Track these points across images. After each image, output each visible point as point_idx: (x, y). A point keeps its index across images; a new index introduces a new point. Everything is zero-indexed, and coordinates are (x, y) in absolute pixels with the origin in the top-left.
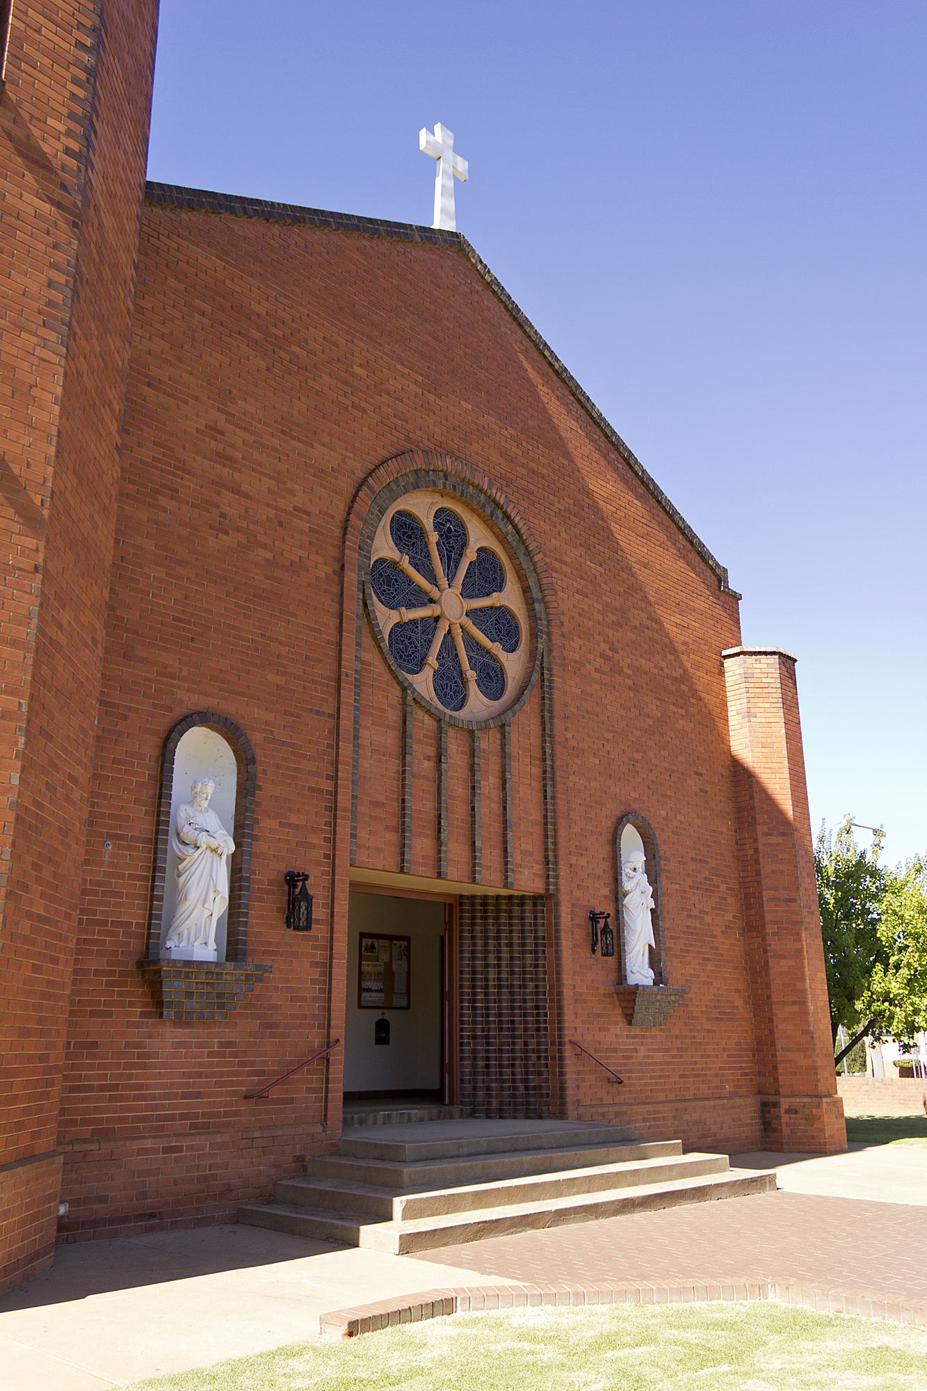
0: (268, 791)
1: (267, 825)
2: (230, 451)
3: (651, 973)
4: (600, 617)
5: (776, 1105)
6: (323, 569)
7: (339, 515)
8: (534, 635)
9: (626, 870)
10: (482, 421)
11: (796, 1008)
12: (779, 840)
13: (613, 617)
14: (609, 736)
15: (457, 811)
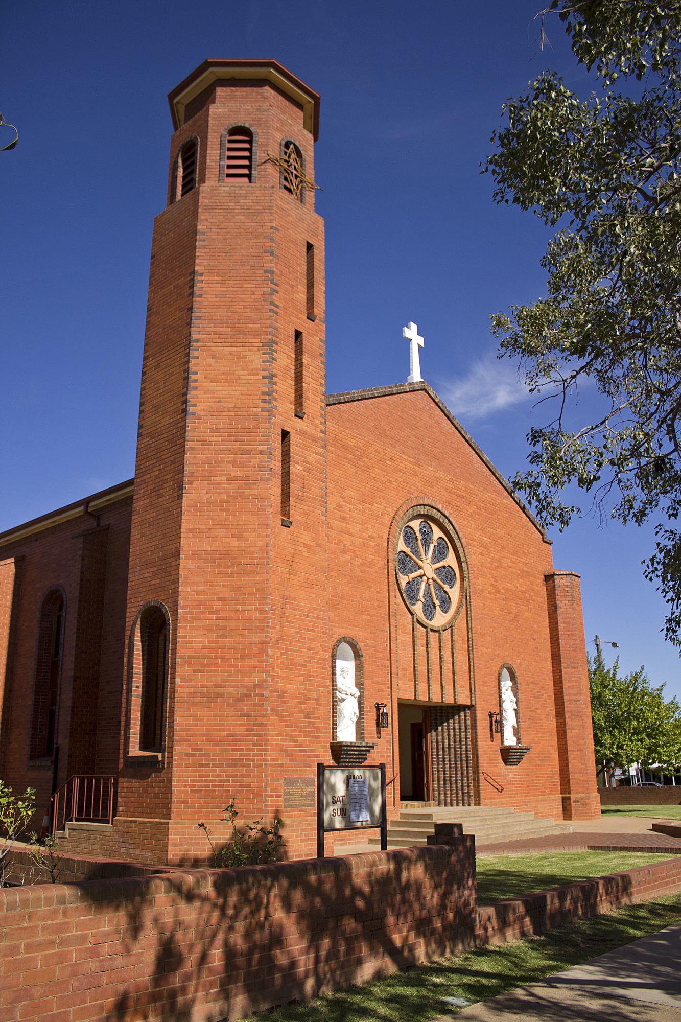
0: (368, 667)
1: (367, 682)
2: (345, 515)
3: (515, 739)
4: (489, 565)
5: (569, 798)
6: (382, 563)
7: (385, 537)
8: (462, 579)
9: (503, 690)
10: (437, 475)
11: (579, 753)
12: (572, 671)
13: (495, 564)
14: (495, 625)
15: (435, 669)
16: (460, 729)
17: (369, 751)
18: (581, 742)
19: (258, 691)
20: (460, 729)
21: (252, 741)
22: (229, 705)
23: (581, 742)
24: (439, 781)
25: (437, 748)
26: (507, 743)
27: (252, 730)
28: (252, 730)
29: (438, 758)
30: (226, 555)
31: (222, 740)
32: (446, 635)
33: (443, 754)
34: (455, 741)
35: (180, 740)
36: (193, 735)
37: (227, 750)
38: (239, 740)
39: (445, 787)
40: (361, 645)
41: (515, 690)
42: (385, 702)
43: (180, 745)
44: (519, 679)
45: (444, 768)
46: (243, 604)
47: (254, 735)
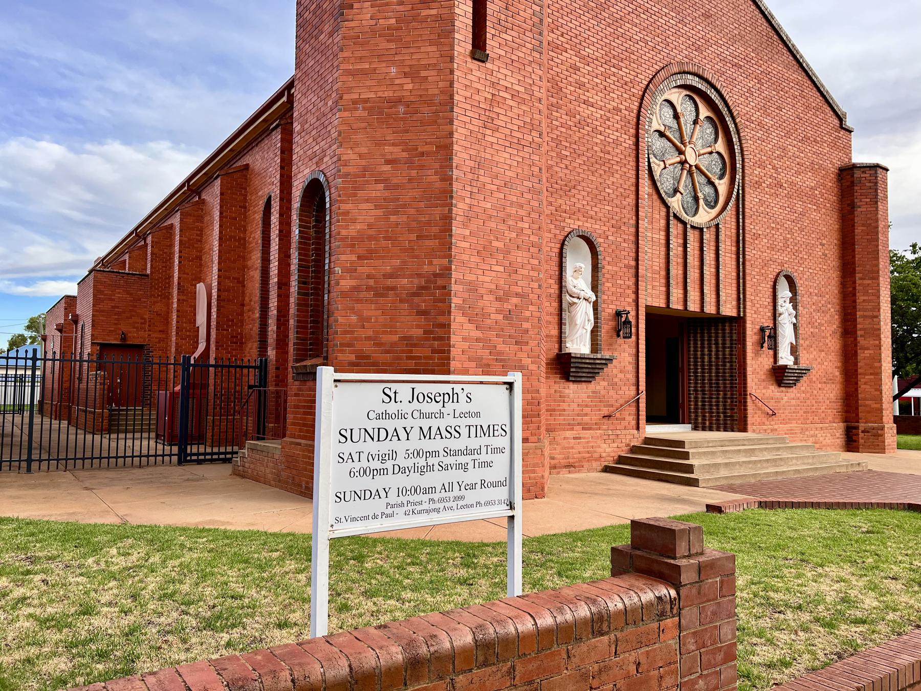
3: (792, 358)
5: (857, 428)
9: (780, 302)
16: (724, 344)
17: (606, 364)
18: (876, 364)
19: (440, 282)
20: (724, 344)
21: (431, 346)
22: (401, 301)
23: (876, 364)
24: (696, 402)
25: (696, 365)
26: (781, 362)
27: (431, 332)
28: (431, 332)
29: (696, 376)
30: (399, 101)
31: (393, 344)
32: (708, 236)
33: (703, 373)
34: (717, 358)
35: (342, 345)
36: (356, 339)
37: (399, 358)
38: (415, 345)
39: (704, 409)
40: (599, 241)
41: (794, 300)
42: (628, 309)
43: (342, 351)
44: (800, 290)
45: (703, 387)
46: (422, 167)
47: (434, 339)
